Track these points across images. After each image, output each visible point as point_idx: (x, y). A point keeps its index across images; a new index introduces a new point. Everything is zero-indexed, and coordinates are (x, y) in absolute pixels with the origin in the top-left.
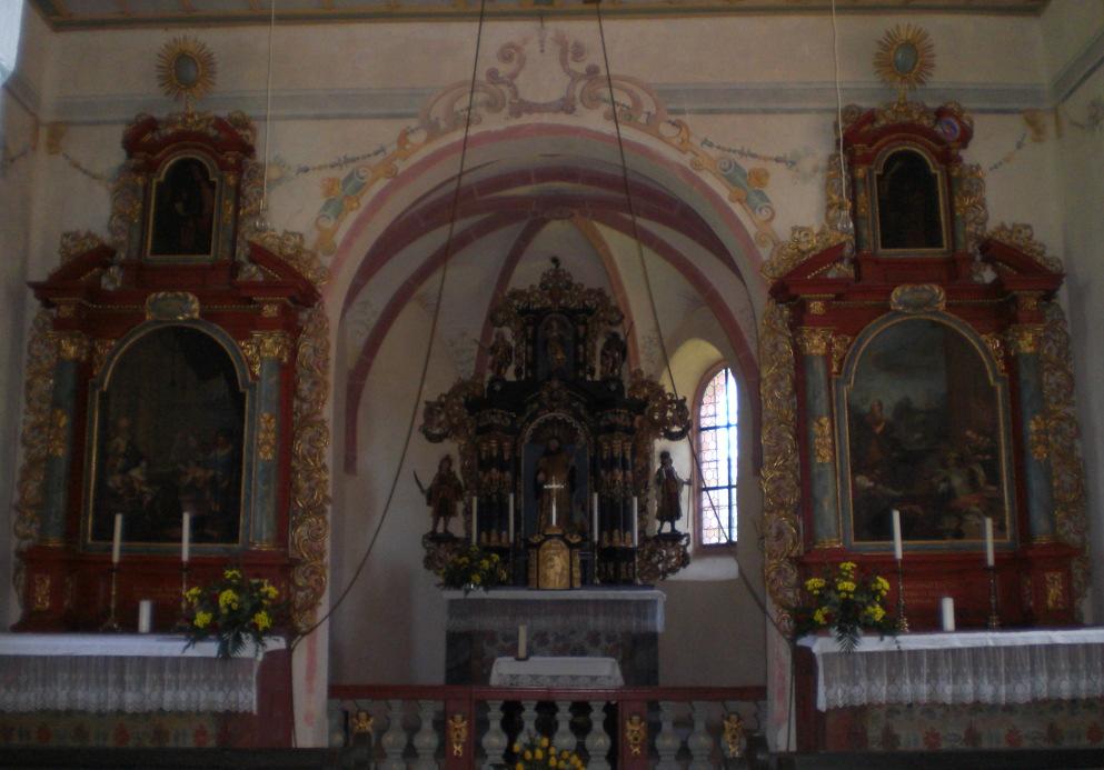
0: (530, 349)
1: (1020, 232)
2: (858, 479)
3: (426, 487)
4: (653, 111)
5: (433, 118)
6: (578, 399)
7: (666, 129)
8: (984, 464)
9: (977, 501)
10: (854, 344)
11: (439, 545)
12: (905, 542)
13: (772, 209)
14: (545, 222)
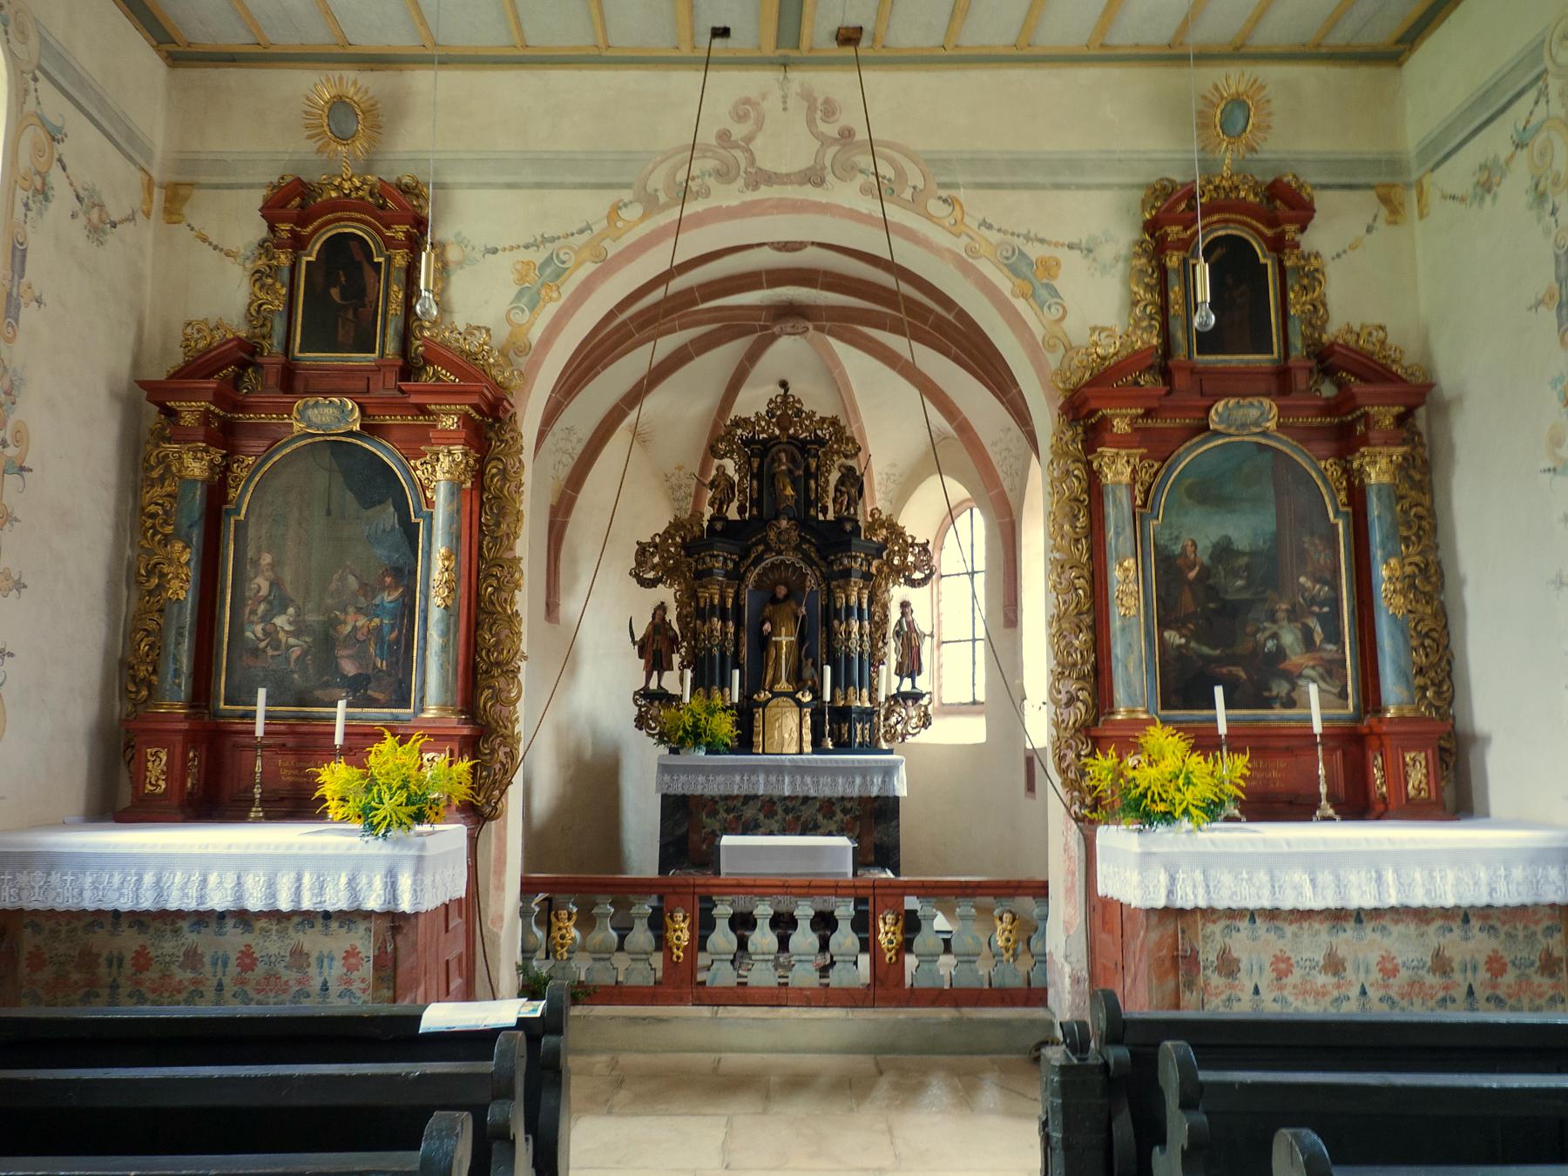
0: (755, 483)
1: (1370, 334)
2: (1166, 634)
3: (637, 638)
4: (920, 185)
5: (650, 189)
6: (809, 542)
7: (935, 207)
8: (1321, 618)
9: (1311, 663)
10: (1163, 472)
11: (651, 703)
12: (1231, 712)
13: (1064, 308)
14: (774, 338)
